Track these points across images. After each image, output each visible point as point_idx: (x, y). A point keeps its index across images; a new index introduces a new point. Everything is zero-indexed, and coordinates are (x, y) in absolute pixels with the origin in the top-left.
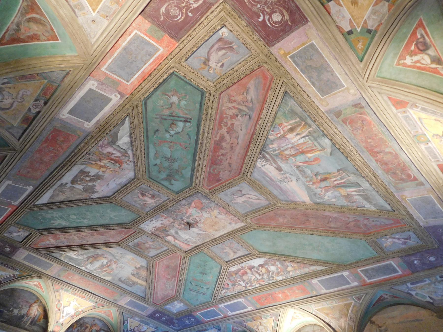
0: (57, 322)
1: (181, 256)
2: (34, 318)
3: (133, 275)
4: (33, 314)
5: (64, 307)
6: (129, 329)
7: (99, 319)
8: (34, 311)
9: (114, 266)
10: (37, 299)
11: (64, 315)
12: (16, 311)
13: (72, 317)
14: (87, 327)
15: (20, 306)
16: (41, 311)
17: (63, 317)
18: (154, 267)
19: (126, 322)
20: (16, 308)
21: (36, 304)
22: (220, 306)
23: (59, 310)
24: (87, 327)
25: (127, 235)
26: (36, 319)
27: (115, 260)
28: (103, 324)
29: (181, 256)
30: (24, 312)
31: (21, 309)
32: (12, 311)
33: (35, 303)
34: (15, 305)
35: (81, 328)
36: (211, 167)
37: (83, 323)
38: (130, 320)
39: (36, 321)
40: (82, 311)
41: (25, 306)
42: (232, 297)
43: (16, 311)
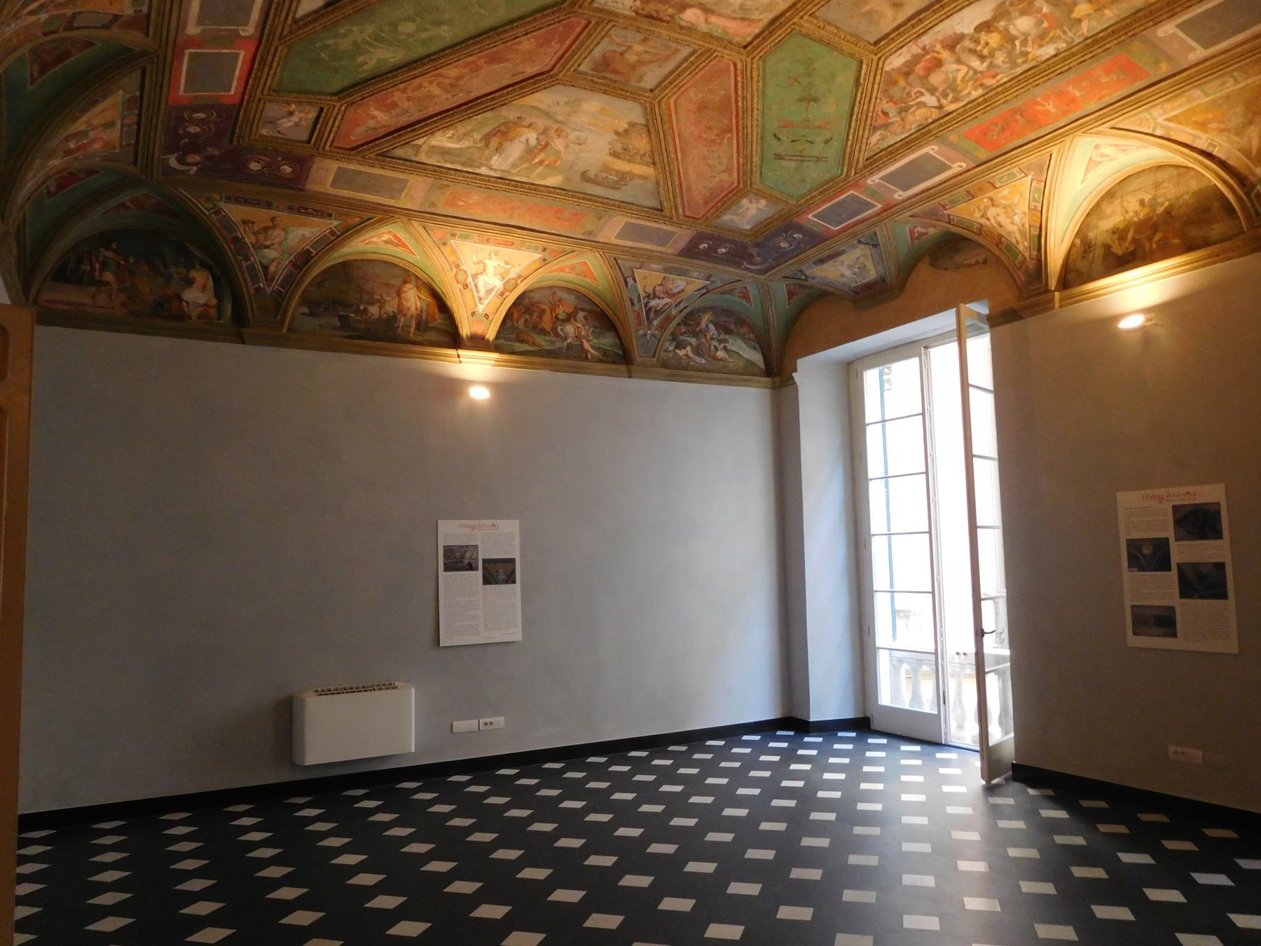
0: (473, 314)
1: (735, 65)
2: (419, 316)
3: (615, 154)
4: (413, 308)
5: (475, 277)
6: (643, 295)
7: (563, 288)
8: (413, 300)
9: (558, 144)
10: (407, 275)
11: (482, 294)
12: (374, 310)
13: (502, 294)
14: (544, 311)
15: (377, 297)
16: (425, 296)
17: (480, 299)
18: (665, 118)
19: (630, 280)
20: (371, 304)
21: (408, 286)
22: (869, 182)
23: (466, 286)
24: (544, 311)
25: (568, 42)
26: (424, 317)
27: (555, 126)
28: (577, 298)
29: (735, 65)
30: (391, 307)
31: (381, 303)
32: (365, 310)
33: (405, 282)
34: (366, 298)
35: (531, 315)
36: (1099, 163)
37: (532, 304)
38: (637, 273)
39: (427, 322)
40: (519, 276)
41: (388, 295)
42: (902, 146)
43: (374, 310)
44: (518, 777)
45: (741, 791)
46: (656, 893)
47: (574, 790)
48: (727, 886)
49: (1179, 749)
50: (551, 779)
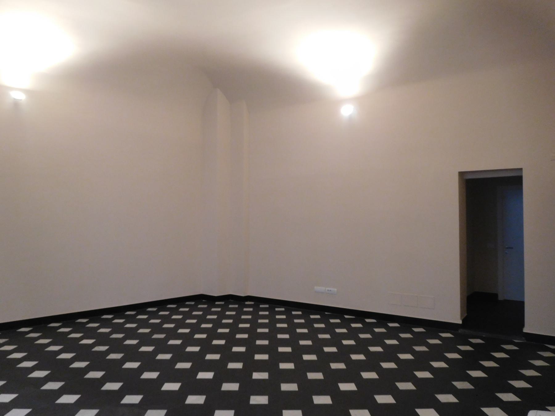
44: (87, 323)
45: (197, 336)
46: (194, 371)
47: (118, 329)
48: (200, 350)
49: (329, 289)
50: (106, 323)
